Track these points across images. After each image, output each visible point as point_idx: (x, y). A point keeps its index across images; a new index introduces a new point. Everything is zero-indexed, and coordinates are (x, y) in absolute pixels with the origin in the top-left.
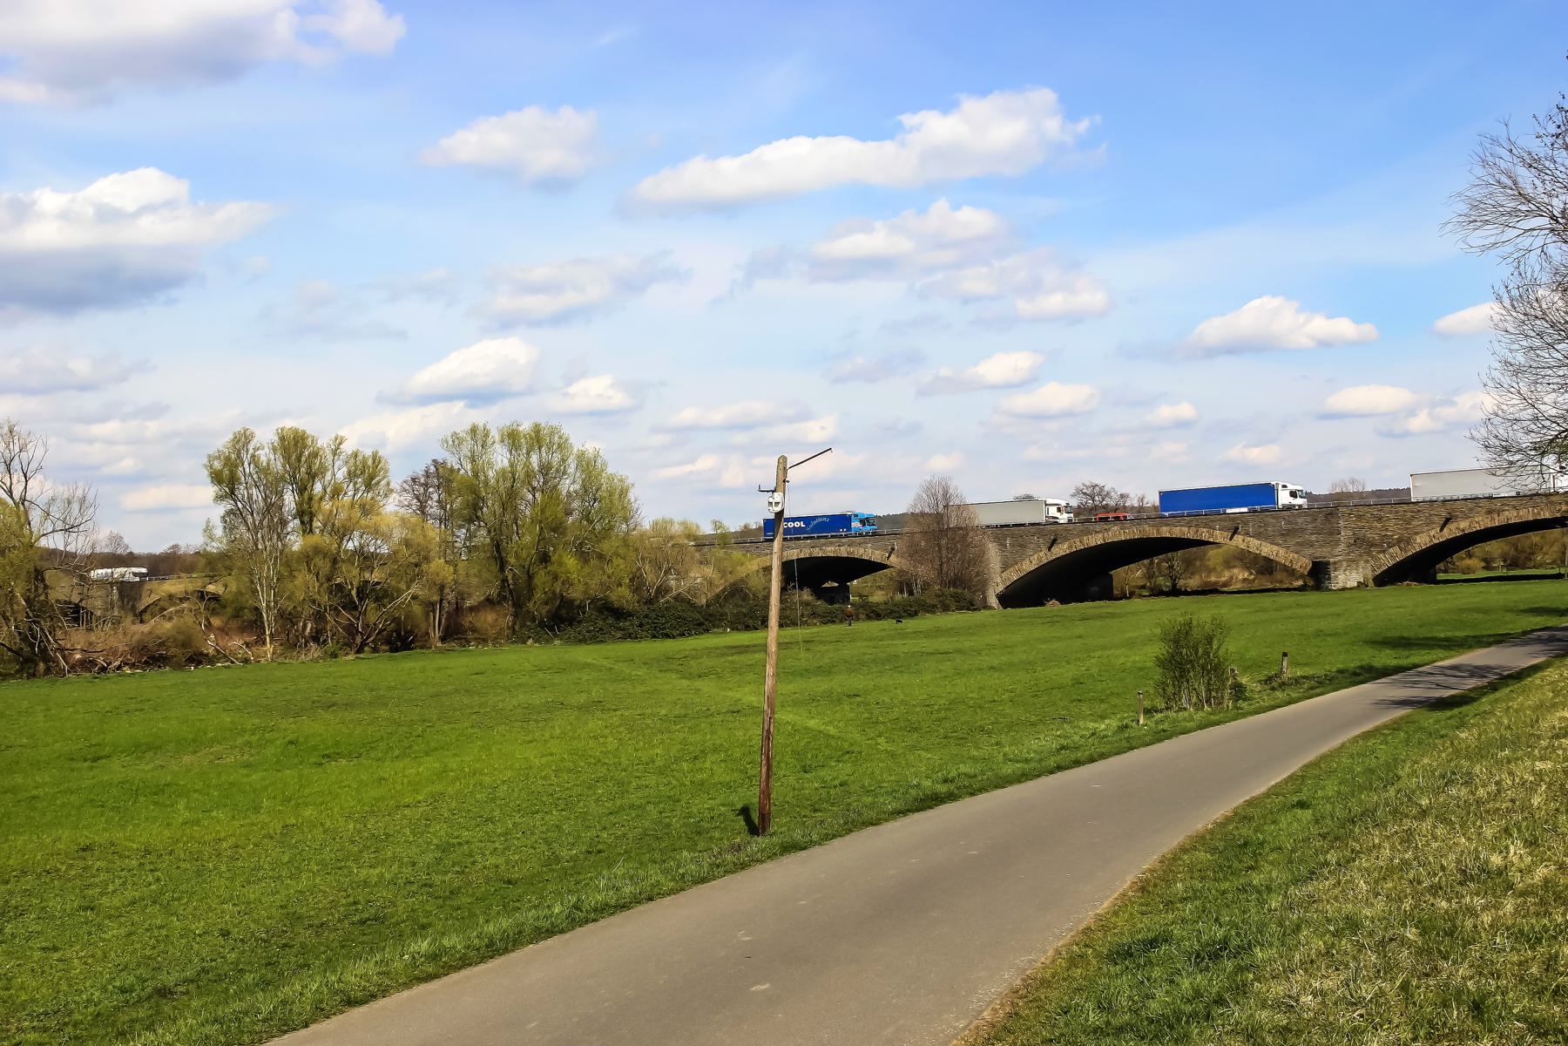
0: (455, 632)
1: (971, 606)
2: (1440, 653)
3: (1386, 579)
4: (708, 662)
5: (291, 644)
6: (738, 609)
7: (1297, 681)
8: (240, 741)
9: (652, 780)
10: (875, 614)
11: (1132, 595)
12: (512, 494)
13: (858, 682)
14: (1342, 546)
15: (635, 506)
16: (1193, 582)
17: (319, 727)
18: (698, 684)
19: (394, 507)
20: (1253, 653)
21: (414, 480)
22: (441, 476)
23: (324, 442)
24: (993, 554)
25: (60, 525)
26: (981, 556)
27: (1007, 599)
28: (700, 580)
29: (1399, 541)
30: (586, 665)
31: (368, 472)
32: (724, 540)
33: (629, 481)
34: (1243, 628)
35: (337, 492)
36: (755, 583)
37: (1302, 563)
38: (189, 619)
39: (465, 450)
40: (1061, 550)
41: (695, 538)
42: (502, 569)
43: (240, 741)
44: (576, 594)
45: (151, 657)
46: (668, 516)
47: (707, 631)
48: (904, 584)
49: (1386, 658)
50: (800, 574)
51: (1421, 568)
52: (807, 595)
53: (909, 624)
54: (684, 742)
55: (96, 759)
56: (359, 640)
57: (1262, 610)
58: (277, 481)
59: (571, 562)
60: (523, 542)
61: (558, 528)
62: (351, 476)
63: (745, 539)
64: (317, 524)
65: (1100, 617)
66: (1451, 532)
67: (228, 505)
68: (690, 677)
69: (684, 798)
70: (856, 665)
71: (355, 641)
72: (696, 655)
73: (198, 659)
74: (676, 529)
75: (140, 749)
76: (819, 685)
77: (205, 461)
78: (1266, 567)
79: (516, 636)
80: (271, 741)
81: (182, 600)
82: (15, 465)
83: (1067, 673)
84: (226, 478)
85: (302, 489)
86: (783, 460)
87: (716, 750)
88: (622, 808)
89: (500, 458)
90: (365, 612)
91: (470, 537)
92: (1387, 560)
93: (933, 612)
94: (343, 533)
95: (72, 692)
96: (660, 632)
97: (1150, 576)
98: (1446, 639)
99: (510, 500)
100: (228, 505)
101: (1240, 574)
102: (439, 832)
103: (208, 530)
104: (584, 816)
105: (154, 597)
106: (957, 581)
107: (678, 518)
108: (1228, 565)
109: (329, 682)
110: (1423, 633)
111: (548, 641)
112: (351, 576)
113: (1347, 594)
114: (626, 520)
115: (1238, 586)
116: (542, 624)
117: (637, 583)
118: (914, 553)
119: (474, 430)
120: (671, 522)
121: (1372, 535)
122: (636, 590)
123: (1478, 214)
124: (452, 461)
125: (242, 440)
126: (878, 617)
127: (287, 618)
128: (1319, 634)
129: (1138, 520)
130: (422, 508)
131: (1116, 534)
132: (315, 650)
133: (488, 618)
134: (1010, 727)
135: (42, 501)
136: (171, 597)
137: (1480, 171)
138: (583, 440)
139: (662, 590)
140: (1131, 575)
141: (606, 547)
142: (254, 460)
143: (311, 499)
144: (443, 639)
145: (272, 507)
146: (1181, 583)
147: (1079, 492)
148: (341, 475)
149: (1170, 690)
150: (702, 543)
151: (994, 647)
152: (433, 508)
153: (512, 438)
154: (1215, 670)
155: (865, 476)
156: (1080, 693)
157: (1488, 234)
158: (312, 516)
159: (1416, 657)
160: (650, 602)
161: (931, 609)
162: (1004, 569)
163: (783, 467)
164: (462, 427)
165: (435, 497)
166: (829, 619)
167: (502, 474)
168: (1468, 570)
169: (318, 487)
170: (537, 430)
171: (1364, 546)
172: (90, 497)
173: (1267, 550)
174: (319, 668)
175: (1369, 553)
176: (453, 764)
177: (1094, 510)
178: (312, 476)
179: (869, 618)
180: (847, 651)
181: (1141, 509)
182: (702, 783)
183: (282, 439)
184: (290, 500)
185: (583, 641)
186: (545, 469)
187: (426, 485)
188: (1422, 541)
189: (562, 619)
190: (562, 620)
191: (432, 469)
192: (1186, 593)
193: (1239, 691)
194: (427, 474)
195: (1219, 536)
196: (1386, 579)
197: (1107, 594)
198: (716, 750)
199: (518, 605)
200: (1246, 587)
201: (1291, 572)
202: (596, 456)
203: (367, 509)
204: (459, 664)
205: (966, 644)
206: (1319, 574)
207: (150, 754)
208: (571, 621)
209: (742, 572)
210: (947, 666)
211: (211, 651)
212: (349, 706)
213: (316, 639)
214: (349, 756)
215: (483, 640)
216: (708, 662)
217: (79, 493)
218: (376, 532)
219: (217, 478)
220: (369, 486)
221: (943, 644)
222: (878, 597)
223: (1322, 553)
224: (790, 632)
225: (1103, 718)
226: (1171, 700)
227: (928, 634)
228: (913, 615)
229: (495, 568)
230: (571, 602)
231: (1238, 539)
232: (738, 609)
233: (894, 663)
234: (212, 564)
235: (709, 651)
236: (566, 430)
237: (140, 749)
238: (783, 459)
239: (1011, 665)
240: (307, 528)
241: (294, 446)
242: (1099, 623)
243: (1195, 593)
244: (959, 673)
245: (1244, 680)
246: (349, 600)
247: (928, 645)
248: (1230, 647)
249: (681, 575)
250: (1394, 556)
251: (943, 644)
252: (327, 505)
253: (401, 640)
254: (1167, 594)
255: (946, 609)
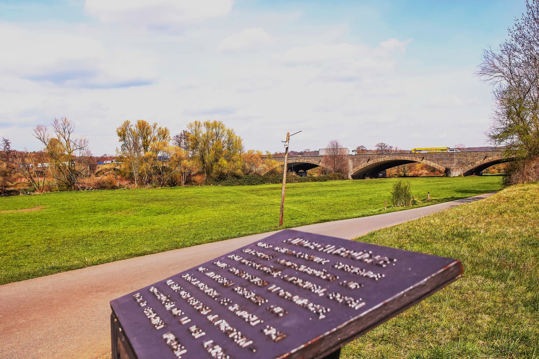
0: (189, 182)
1: (343, 179)
2: (474, 194)
3: (467, 174)
4: (265, 192)
5: (142, 184)
6: (273, 177)
7: (432, 200)
8: (133, 209)
9: (250, 221)
10: (314, 180)
11: (392, 176)
12: (207, 141)
13: (308, 198)
14: (455, 164)
15: (243, 146)
16: (411, 174)
17: (154, 206)
18: (261, 197)
19: (171, 144)
20: (423, 193)
21: (177, 136)
22: (185, 136)
23: (151, 124)
24: (350, 163)
25: (78, 147)
26: (346, 164)
27: (354, 177)
28: (262, 168)
29: (471, 163)
30: (228, 192)
31: (164, 134)
32: (269, 157)
33: (241, 138)
34: (416, 187)
35: (154, 140)
36: (279, 170)
37: (442, 169)
38: (112, 176)
39: (193, 128)
40: (371, 162)
41: (261, 156)
42: (204, 163)
43: (133, 209)
44: (225, 171)
45: (101, 186)
46: (253, 149)
47: (264, 183)
48: (324, 171)
49: (459, 195)
50: (292, 167)
51: (478, 171)
52: (294, 174)
53: (325, 183)
54: (258, 212)
55: (95, 212)
56: (162, 183)
57: (429, 182)
58: (138, 136)
59: (225, 162)
60: (209, 157)
61: (221, 152)
62: (159, 134)
63: (278, 156)
64: (149, 149)
65: (381, 182)
66: (486, 161)
67: (123, 143)
68: (259, 196)
69: (259, 225)
70: (306, 194)
71: (161, 184)
72: (261, 190)
73: (114, 188)
74: (255, 153)
75: (107, 210)
76: (296, 198)
77: (116, 130)
78: (433, 170)
79: (207, 183)
80: (142, 209)
81: (109, 170)
82: (66, 130)
83: (368, 197)
84: (122, 135)
85: (144, 138)
86: (288, 134)
87: (267, 214)
88: (242, 227)
89: (204, 130)
90: (163, 176)
91: (194, 153)
92: (467, 169)
93: (332, 180)
94: (157, 151)
95: (82, 194)
96: (250, 183)
97: (398, 172)
98: (478, 191)
99: (206, 143)
100: (123, 143)
101: (425, 171)
102: (193, 231)
103: (117, 150)
104: (232, 228)
105: (100, 169)
106: (339, 171)
107: (256, 149)
108: (422, 169)
109: (155, 194)
110: (472, 189)
111: (217, 185)
112: (160, 164)
113: (455, 178)
114: (240, 150)
115: (424, 175)
116: (215, 180)
117: (244, 169)
118: (326, 162)
119: (196, 122)
120: (254, 151)
121: (463, 161)
122: (243, 171)
123: (484, 71)
124: (189, 131)
125: (127, 123)
126: (315, 181)
127: (141, 176)
128: (442, 189)
129: (395, 154)
130: (180, 145)
131: (388, 158)
132: (149, 186)
133: (198, 178)
134: (350, 210)
135: (73, 140)
136: (106, 169)
137: (484, 60)
138: (228, 126)
139: (251, 171)
140: (393, 171)
141: (234, 157)
142: (130, 129)
143: (147, 141)
144: (185, 184)
145: (135, 144)
146: (407, 174)
147: (378, 145)
148: (156, 134)
149: (395, 201)
150: (263, 157)
151: (348, 190)
152: (183, 145)
153: (207, 125)
154: (408, 196)
155: (312, 140)
156: (370, 202)
157: (486, 77)
158: (147, 146)
159: (468, 195)
160: (247, 174)
161: (331, 179)
162: (354, 167)
163: (288, 135)
164: (193, 121)
165: (183, 141)
166: (300, 181)
167: (204, 136)
168: (494, 172)
169: (149, 138)
170: (215, 122)
171: (461, 164)
172: (87, 140)
173: (432, 164)
174: (150, 191)
175: (462, 166)
176: (194, 216)
177: (382, 150)
178: (147, 134)
179: (312, 181)
180: (307, 190)
181: (396, 151)
182: (263, 222)
183: (139, 123)
184: (141, 141)
185: (227, 185)
186: (217, 134)
187: (181, 138)
188: (478, 163)
189: (221, 179)
190: (221, 179)
191: (183, 133)
192: (408, 177)
193: (414, 203)
194: (181, 135)
195: (418, 160)
196: (467, 174)
197: (384, 176)
198: (267, 214)
199: (208, 174)
200: (427, 175)
201: (440, 172)
202: (233, 130)
203: (165, 145)
204: (191, 191)
205: (341, 189)
206: (447, 172)
207: (109, 212)
208: (224, 179)
209: (274, 166)
210: (334, 194)
211: (118, 185)
212: (162, 200)
213: (149, 182)
214: (164, 214)
215: (197, 185)
216: (265, 192)
217: (84, 139)
218: (168, 152)
219: (120, 135)
220: (164, 137)
221: (334, 189)
222: (316, 175)
223: (448, 166)
224: (289, 185)
225: (376, 208)
226: (395, 204)
227: (329, 186)
228: (326, 180)
229: (201, 163)
230: (224, 174)
231: (424, 161)
232: (273, 177)
233: (319, 194)
234: (120, 159)
235: (265, 189)
236: (224, 123)
237: (107, 210)
238: (288, 134)
239: (353, 194)
240: (146, 150)
241: (143, 126)
242: (380, 184)
243: (411, 177)
244: (337, 196)
245: (415, 199)
246: (159, 172)
247: (330, 189)
248: (413, 192)
249: (257, 167)
250: (471, 167)
251: (334, 189)
252: (152, 143)
253: (173, 183)
254: (402, 177)
255: (336, 179)
